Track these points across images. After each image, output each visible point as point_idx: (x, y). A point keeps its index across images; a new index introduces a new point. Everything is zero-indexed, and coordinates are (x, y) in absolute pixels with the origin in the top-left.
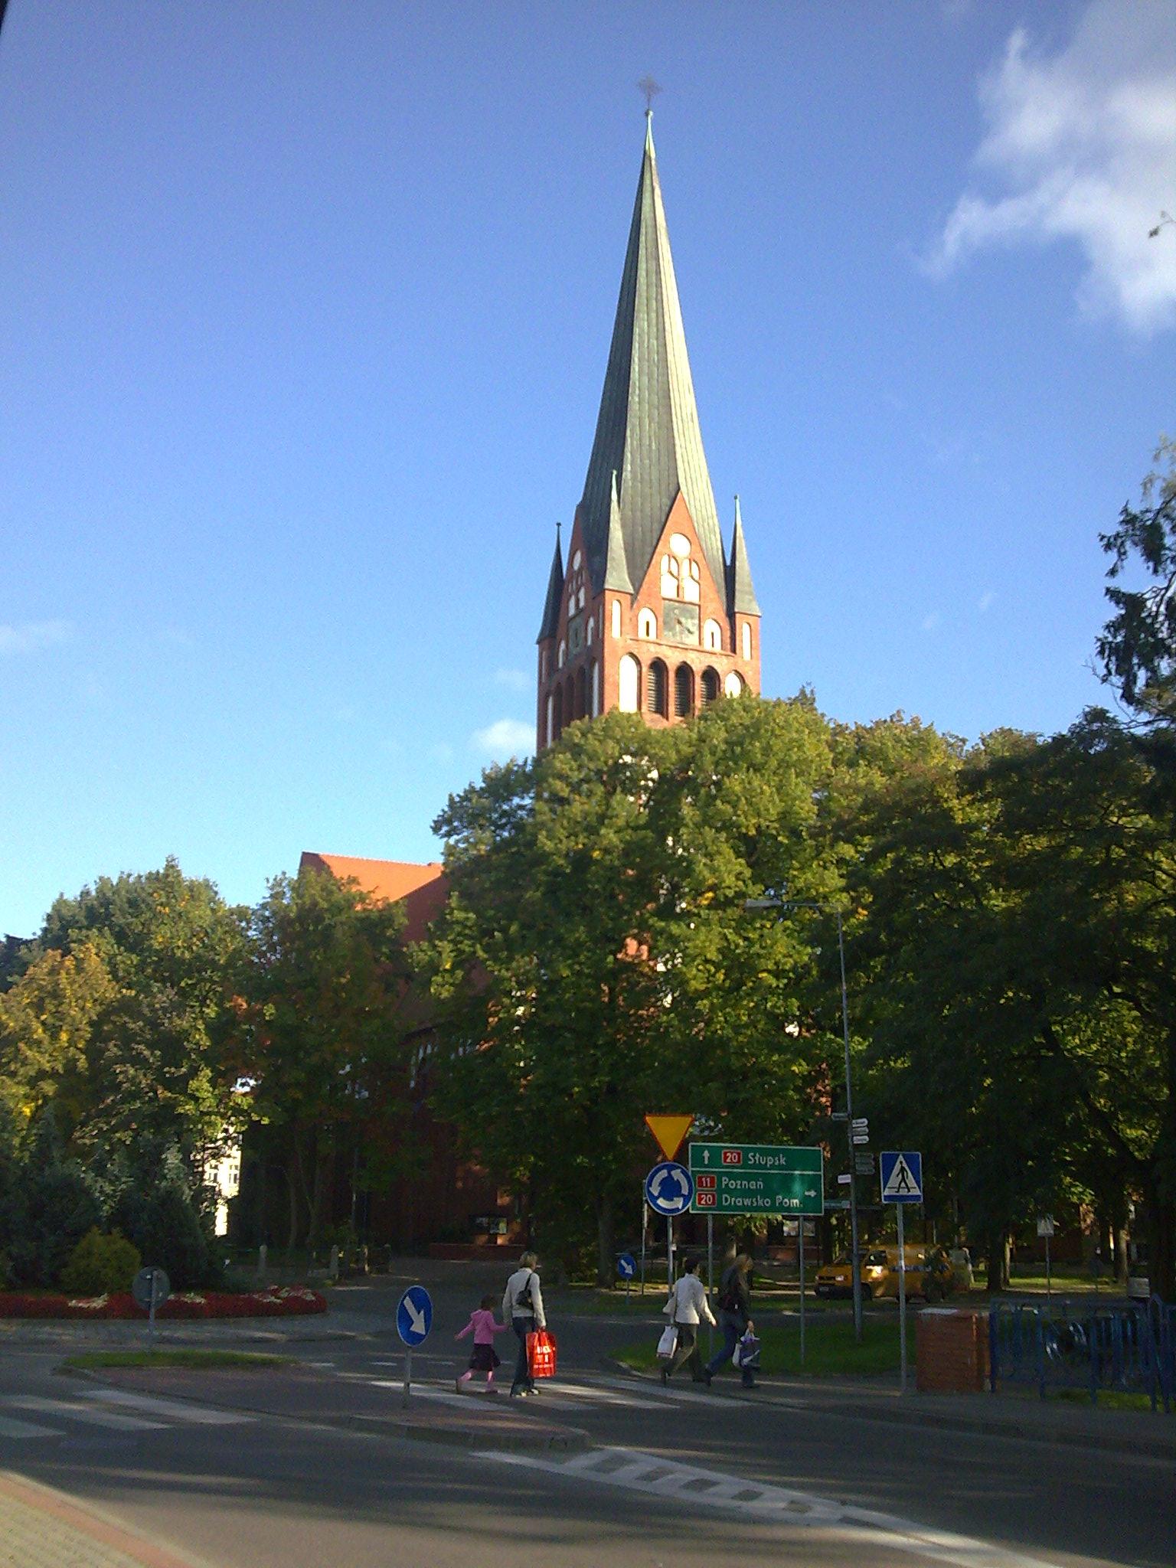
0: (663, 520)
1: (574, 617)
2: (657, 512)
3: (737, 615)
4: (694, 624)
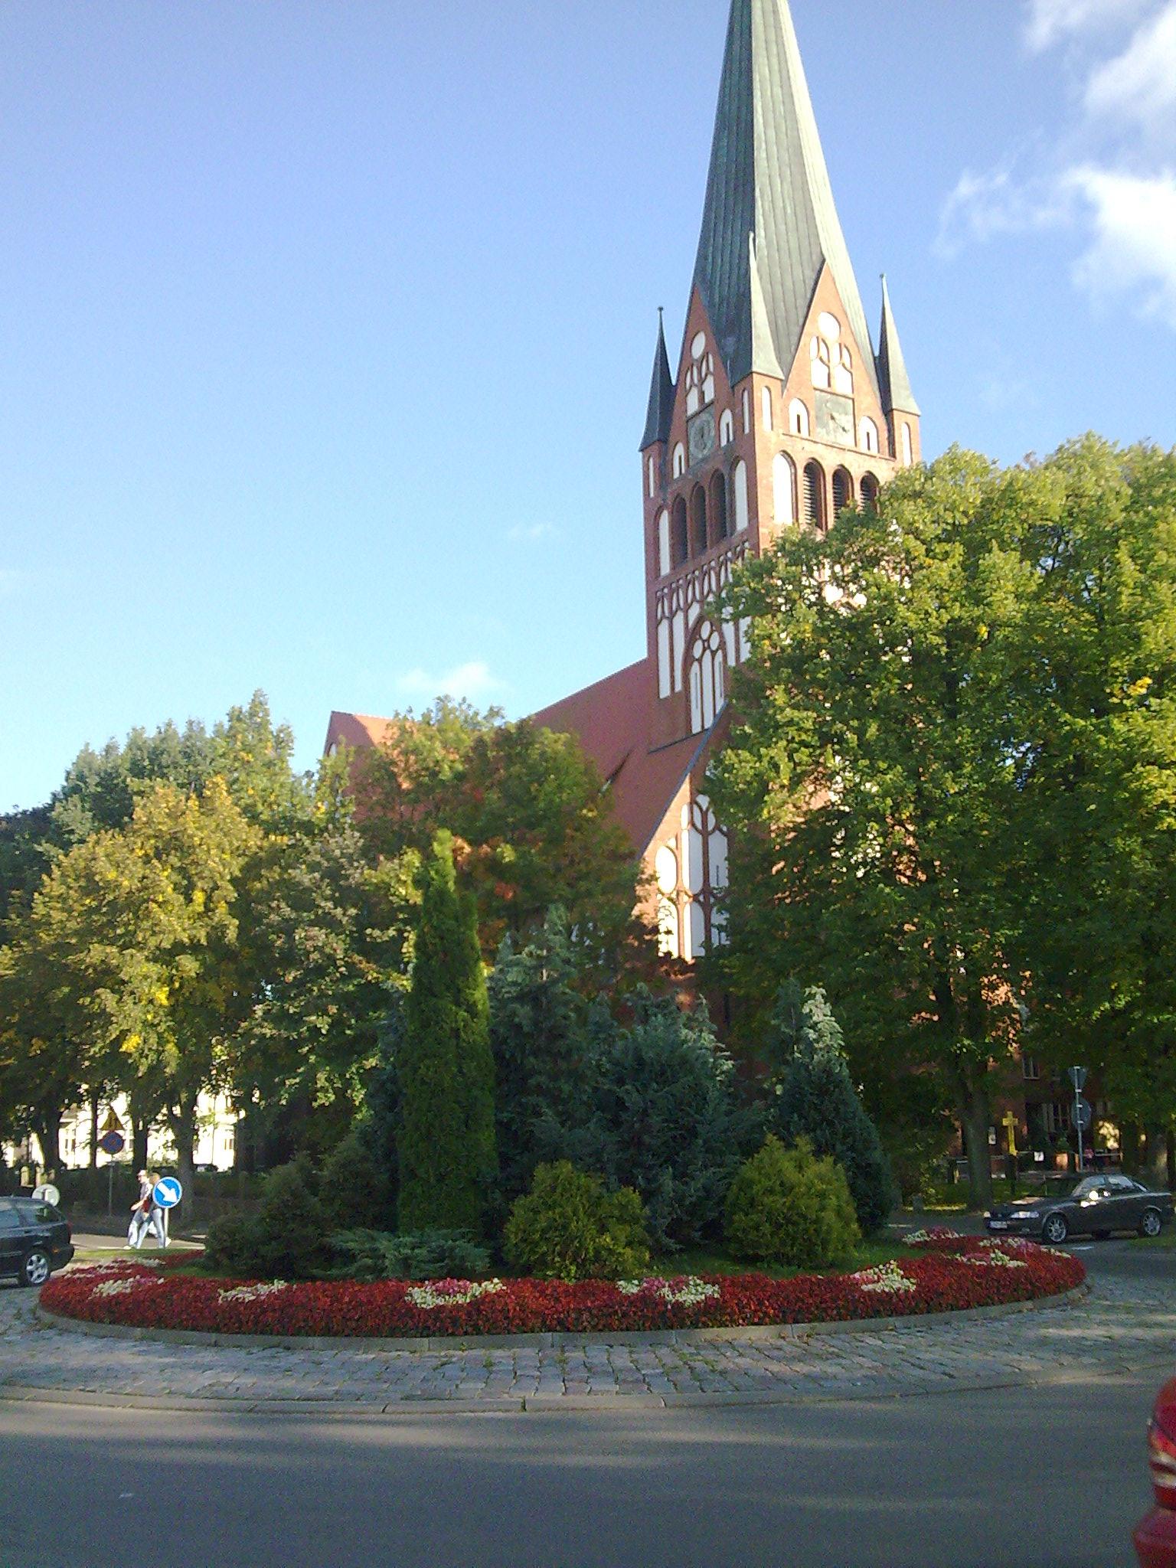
0: (809, 296)
1: (697, 414)
3: (895, 412)
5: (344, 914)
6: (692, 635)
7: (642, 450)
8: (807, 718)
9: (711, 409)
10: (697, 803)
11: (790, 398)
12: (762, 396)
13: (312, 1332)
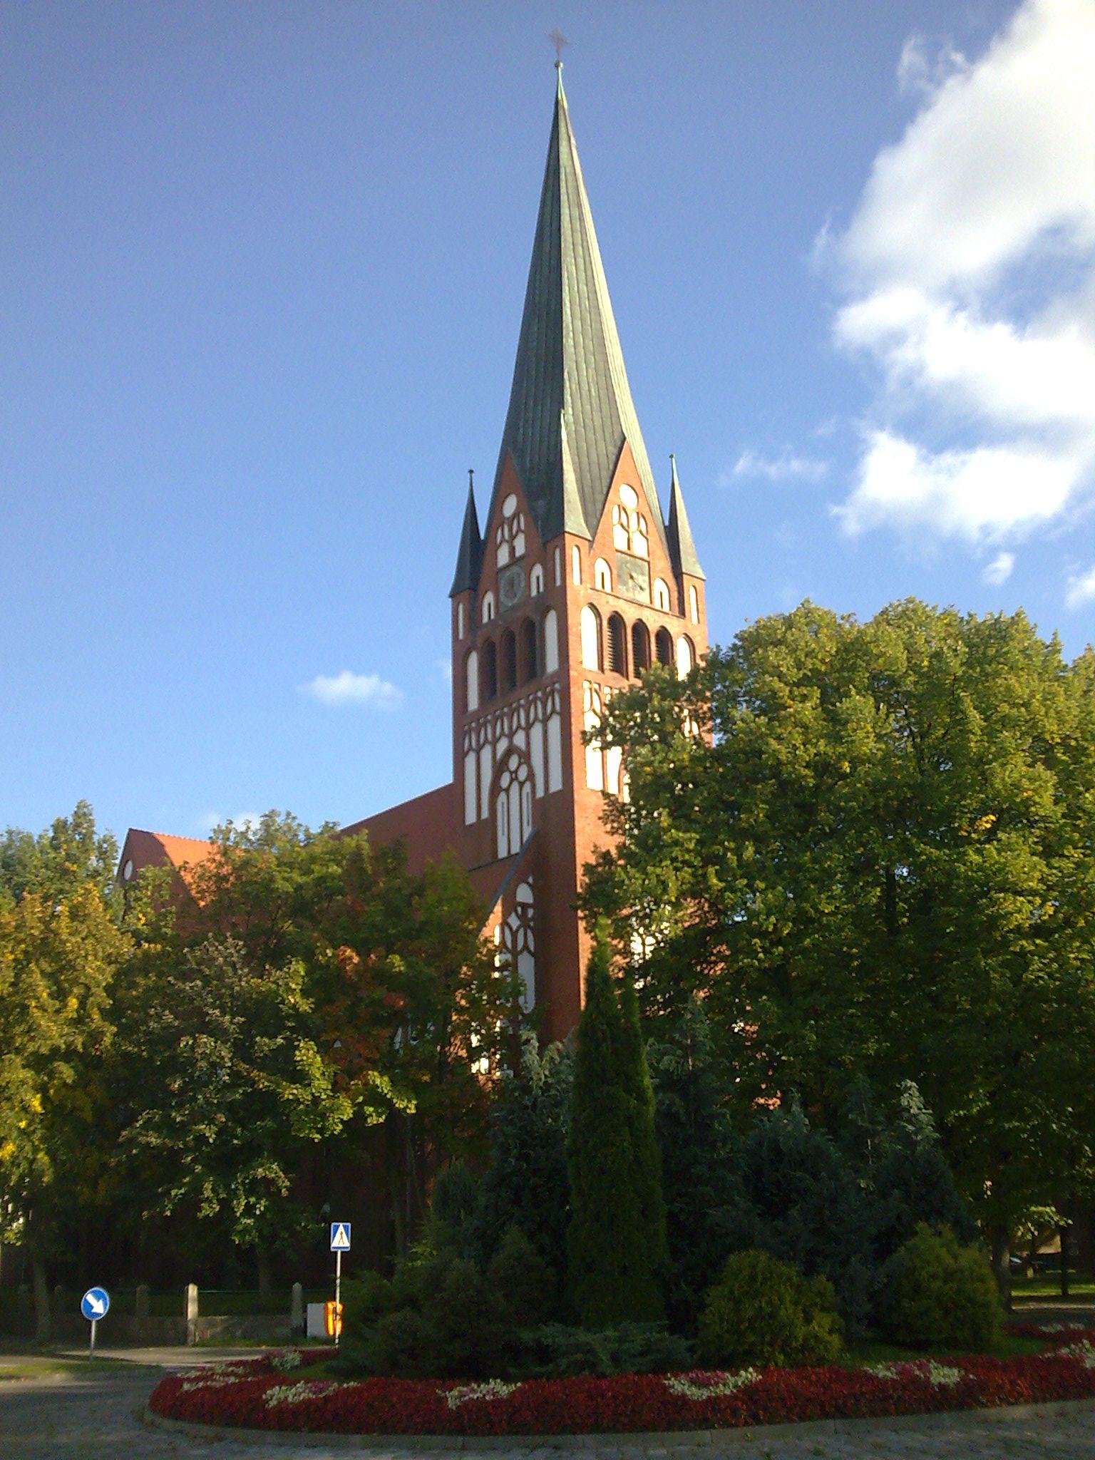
1: (506, 567)
2: (603, 460)
4: (644, 581)
5: (231, 1023)
6: (500, 767)
7: (451, 596)
8: (690, 839)
9: (523, 563)
10: (508, 925)
11: (595, 557)
12: (573, 554)
13: (577, 1429)
